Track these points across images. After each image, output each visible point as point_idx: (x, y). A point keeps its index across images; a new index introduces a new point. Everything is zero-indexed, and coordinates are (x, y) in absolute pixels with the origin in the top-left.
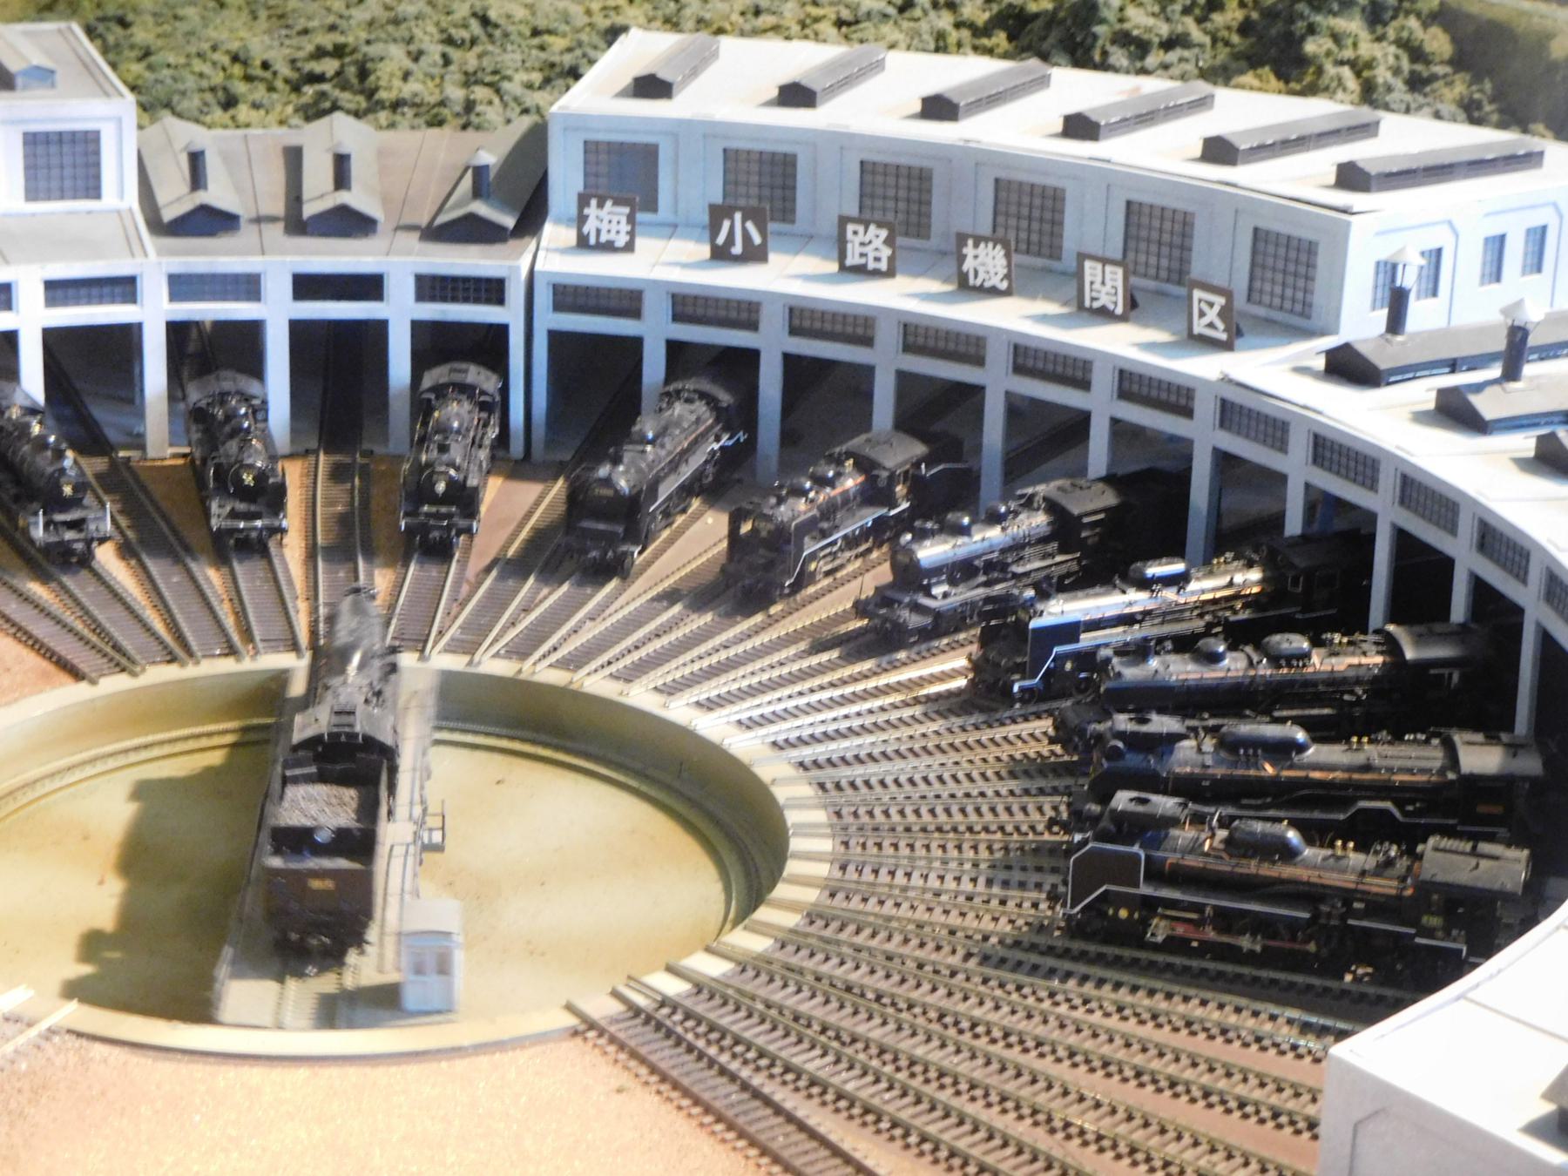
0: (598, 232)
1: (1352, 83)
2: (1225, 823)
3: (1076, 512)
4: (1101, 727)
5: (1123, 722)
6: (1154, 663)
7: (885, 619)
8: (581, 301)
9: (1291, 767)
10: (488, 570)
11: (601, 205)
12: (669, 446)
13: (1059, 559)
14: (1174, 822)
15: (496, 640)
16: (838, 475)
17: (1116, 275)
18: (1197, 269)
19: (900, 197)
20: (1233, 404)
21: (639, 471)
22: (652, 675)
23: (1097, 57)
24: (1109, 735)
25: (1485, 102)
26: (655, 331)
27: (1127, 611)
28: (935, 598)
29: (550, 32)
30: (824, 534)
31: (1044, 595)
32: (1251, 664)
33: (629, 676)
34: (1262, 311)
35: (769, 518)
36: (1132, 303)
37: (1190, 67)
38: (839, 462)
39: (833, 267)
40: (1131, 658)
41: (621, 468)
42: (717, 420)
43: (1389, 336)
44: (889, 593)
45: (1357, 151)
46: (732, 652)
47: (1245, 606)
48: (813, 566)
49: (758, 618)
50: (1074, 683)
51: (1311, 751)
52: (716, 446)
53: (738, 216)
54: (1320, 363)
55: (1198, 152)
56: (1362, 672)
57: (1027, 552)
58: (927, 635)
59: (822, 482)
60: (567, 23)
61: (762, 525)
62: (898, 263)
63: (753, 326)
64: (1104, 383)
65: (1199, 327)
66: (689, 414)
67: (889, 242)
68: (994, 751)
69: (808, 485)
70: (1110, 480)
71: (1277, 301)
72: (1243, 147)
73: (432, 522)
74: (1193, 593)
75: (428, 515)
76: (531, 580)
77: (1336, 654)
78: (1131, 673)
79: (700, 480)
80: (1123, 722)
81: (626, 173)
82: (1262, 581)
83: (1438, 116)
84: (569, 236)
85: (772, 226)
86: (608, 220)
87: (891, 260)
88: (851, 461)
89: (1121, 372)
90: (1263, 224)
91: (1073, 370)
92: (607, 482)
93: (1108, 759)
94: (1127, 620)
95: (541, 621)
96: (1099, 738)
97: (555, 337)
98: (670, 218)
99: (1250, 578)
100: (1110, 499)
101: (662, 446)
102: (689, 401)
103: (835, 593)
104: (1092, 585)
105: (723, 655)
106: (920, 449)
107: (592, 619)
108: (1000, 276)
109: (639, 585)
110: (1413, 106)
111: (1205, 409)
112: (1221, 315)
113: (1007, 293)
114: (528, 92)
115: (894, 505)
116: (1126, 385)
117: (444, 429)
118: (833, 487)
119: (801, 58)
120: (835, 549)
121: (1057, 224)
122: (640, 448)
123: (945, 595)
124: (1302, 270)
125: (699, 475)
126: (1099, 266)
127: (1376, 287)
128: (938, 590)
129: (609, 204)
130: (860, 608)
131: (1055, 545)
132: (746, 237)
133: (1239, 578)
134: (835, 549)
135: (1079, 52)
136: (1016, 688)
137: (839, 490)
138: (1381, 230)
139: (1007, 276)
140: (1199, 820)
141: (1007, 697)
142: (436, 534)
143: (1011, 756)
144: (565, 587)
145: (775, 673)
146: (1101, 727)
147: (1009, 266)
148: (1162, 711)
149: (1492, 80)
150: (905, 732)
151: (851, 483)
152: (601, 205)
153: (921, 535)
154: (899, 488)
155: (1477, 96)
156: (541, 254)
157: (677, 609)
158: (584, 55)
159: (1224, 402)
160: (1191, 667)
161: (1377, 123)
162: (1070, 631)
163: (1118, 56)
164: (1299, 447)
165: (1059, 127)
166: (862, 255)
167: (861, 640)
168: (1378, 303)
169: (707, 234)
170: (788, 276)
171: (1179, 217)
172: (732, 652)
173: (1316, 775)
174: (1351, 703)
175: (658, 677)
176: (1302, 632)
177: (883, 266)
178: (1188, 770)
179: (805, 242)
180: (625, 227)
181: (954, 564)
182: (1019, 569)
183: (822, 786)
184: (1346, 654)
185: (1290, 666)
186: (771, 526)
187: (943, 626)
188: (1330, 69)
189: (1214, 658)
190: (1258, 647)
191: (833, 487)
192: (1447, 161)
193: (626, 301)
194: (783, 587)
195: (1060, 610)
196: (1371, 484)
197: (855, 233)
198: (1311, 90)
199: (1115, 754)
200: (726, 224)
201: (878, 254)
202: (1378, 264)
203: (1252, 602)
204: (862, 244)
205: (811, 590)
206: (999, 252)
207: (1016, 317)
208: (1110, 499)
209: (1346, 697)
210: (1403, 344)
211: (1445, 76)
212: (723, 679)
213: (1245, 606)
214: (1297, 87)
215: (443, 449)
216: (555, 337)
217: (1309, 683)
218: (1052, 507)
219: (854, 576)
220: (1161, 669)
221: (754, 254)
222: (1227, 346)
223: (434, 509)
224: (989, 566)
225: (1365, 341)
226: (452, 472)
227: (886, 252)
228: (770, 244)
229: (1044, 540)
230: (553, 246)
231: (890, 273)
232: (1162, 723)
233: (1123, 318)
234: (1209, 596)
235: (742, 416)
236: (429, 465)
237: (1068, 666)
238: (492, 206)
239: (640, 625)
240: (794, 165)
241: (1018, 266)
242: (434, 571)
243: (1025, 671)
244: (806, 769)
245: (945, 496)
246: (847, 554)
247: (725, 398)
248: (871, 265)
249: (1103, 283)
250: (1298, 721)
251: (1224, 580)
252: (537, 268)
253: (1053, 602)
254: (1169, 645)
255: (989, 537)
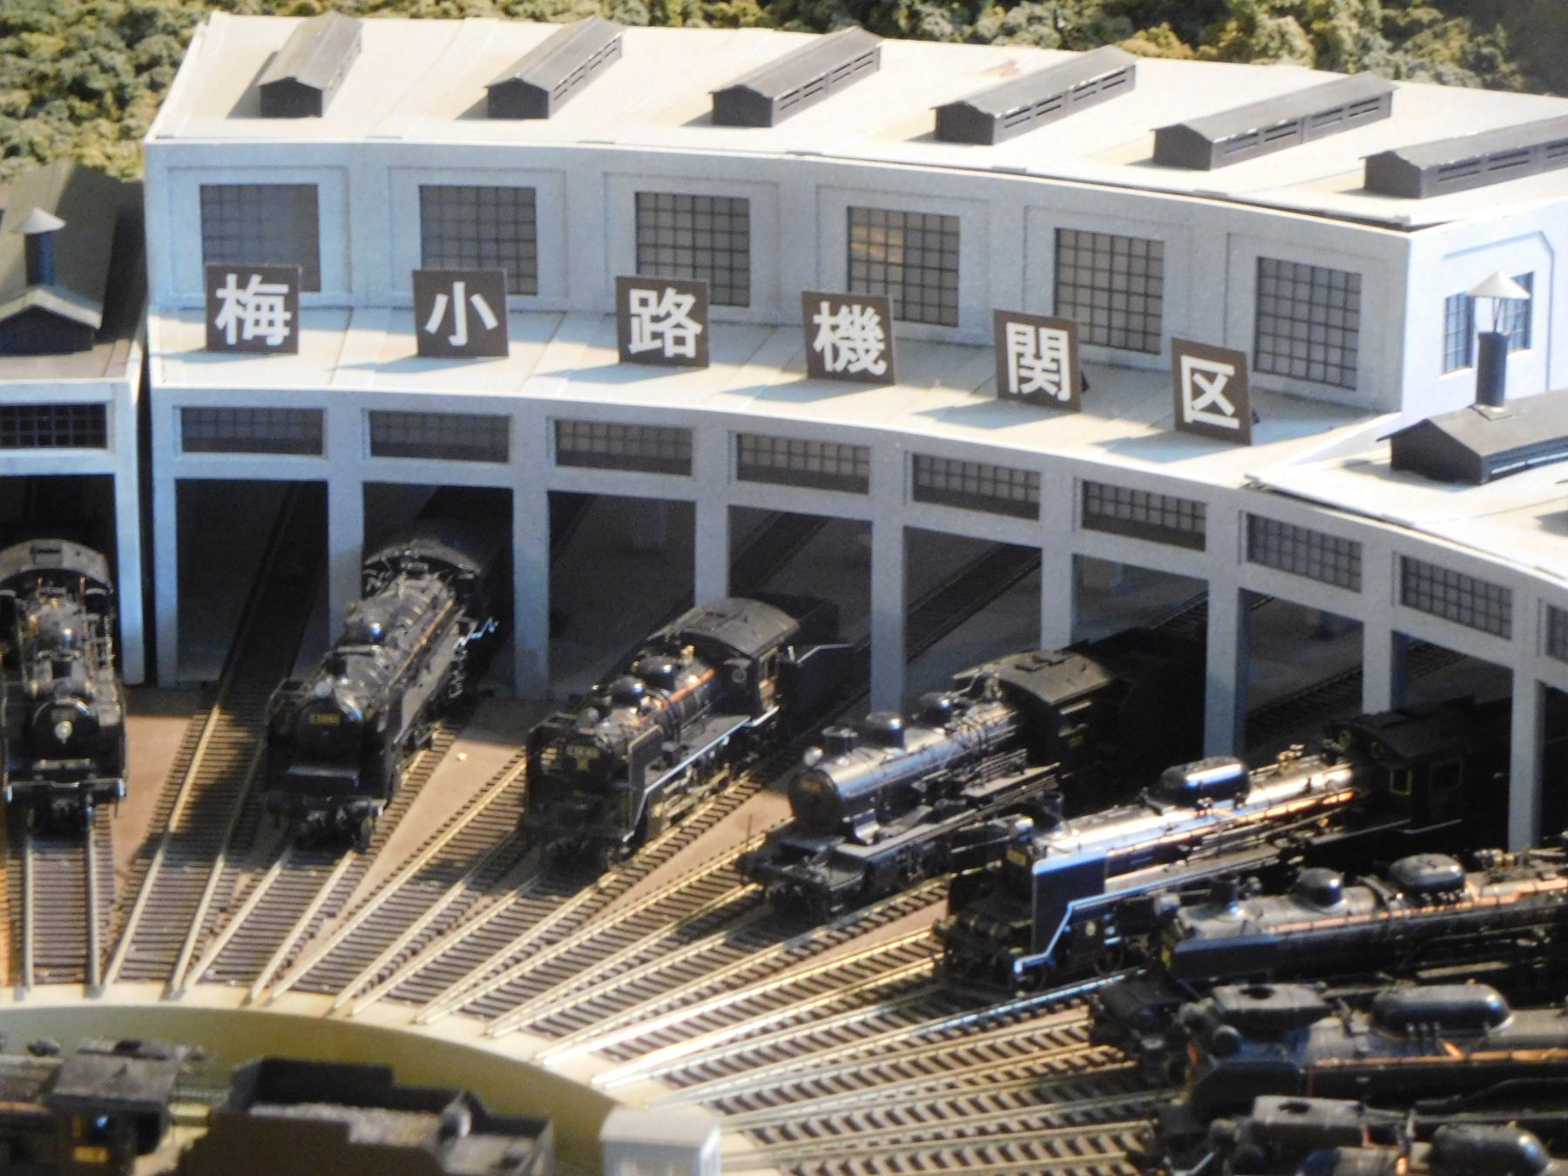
0: (240, 323)
1: (1301, 41)
2: (1423, 1134)
3: (1050, 698)
4: (1200, 1007)
5: (1232, 997)
6: (1239, 912)
7: (791, 881)
8: (226, 432)
9: (1486, 1047)
10: (147, 852)
11: (242, 284)
12: (403, 645)
13: (1030, 772)
14: (1351, 1137)
15: (196, 958)
16: (678, 668)
17: (1057, 343)
18: (1172, 324)
19: (701, 242)
20: (1267, 521)
21: (371, 684)
22: (454, 989)
23: (903, 23)
24: (1212, 1020)
25: (1500, 59)
26: (346, 471)
27: (1166, 840)
28: (861, 843)
29: (29, 28)
30: (671, 760)
31: (1046, 824)
32: (1380, 903)
33: (424, 989)
34: (1277, 383)
35: (587, 741)
36: (1081, 384)
37: (1046, 30)
38: (672, 651)
39: (613, 357)
40: (1203, 906)
41: (344, 681)
42: (459, 601)
43: (1482, 408)
44: (789, 841)
45: (1375, 137)
46: (561, 949)
47: (1333, 822)
48: (657, 810)
49: (586, 895)
50: (1139, 957)
51: (1509, 1021)
52: (463, 641)
53: (459, 288)
54: (1383, 454)
55: (1148, 151)
56: (1540, 903)
57: (986, 764)
58: (856, 899)
59: (658, 682)
60: (53, 13)
61: (577, 752)
62: (711, 345)
63: (499, 453)
64: (1059, 504)
65: (1193, 412)
66: (419, 594)
67: (696, 314)
68: (999, 1067)
69: (638, 686)
70: (1078, 647)
71: (1300, 367)
72: (1217, 140)
73: (54, 784)
74: (1256, 807)
75: (47, 774)
76: (220, 865)
77: (1498, 880)
78: (1211, 929)
79: (446, 694)
80: (1232, 997)
81: (265, 230)
82: (1352, 783)
83: (1439, 79)
84: (196, 333)
85: (511, 301)
86: (254, 305)
87: (701, 340)
88: (690, 648)
89: (1086, 485)
90: (1271, 253)
91: (1013, 490)
92: (329, 704)
93: (1217, 1055)
94: (1166, 854)
95: (254, 922)
96: (1197, 1023)
97: (187, 489)
98: (342, 298)
99: (1333, 779)
100: (1092, 677)
101: (396, 646)
102: (414, 575)
103: (688, 851)
104: (1106, 805)
105: (549, 954)
106: (785, 624)
107: (332, 915)
108: (874, 354)
109: (384, 861)
110: (1404, 69)
111: (1224, 534)
112: (1227, 392)
113: (886, 380)
114: (11, 122)
115: (756, 711)
116: (1095, 506)
117: (48, 640)
118: (672, 689)
119: (755, 52)
120: (684, 781)
121: (948, 271)
122: (365, 649)
123: (877, 838)
124: (1336, 318)
125: (445, 687)
126: (1030, 330)
127: (1447, 336)
128: (865, 832)
129: (255, 279)
130: (746, 867)
131: (1023, 752)
132: (473, 316)
133: (1319, 780)
134: (684, 781)
135: (875, 15)
136: (1018, 967)
137: (680, 692)
138: (1455, 249)
139: (885, 355)
140: (1382, 1136)
141: (1004, 984)
142: (60, 803)
143: (1028, 1069)
144: (276, 871)
145: (637, 974)
146: (1200, 1007)
147: (887, 340)
148: (1285, 977)
149: (1505, 28)
150: (862, 1046)
151: (694, 680)
152: (242, 284)
153: (836, 749)
154: (763, 684)
155: (1486, 50)
156: (155, 365)
157: (457, 890)
158: (94, 60)
159: (1252, 519)
160: (1295, 913)
161: (1390, 95)
162: (1089, 876)
163: (936, 19)
164: (1379, 579)
165: (930, 125)
166: (656, 336)
167: (750, 917)
168: (1451, 359)
169: (410, 318)
170: (542, 373)
171: (1139, 250)
172: (561, 949)
173: (1522, 1055)
174: (1530, 952)
175: (462, 992)
176: (1448, 852)
177: (689, 350)
178: (1335, 1061)
179: (557, 321)
180: (281, 315)
181: (885, 789)
182: (978, 793)
183: (760, 1135)
184: (1513, 879)
185: (1437, 902)
186: (592, 753)
187: (879, 884)
188: (1267, 23)
189: (1325, 898)
190: (1385, 876)
191: (672, 689)
192: (1521, 145)
193: (298, 427)
194: (619, 844)
195: (1071, 844)
196: (1500, 626)
197: (644, 302)
198: (1239, 53)
199: (1226, 1046)
200: (441, 301)
201: (679, 332)
202: (1448, 300)
203: (1342, 815)
204: (656, 319)
205: (651, 848)
206: (871, 318)
207: (910, 412)
208: (1092, 677)
209: (1522, 942)
210: (1505, 417)
211: (1433, 22)
212: (562, 988)
213: (1333, 822)
214: (1213, 51)
215: (61, 670)
216: (187, 489)
217: (1466, 925)
218: (1013, 695)
219: (709, 823)
220: (1252, 918)
221: (487, 345)
222: (1240, 438)
223: (55, 765)
224: (934, 790)
225: (1451, 416)
226: (80, 705)
227: (693, 329)
228: (510, 327)
229: (1006, 746)
230: (168, 351)
231: (700, 361)
232: (1289, 996)
233: (1072, 407)
234: (1280, 810)
235: (488, 596)
236: (44, 696)
237: (1091, 928)
238: (57, 294)
239: (410, 920)
240: (532, 205)
241: (903, 340)
242: (64, 861)
243: (1027, 941)
244: (729, 1112)
245: (826, 695)
246: (698, 791)
247: (468, 566)
248: (671, 350)
249: (1038, 356)
250: (1482, 978)
251: (1298, 785)
252: (156, 382)
253: (1057, 835)
254: (1255, 883)
255: (929, 745)
